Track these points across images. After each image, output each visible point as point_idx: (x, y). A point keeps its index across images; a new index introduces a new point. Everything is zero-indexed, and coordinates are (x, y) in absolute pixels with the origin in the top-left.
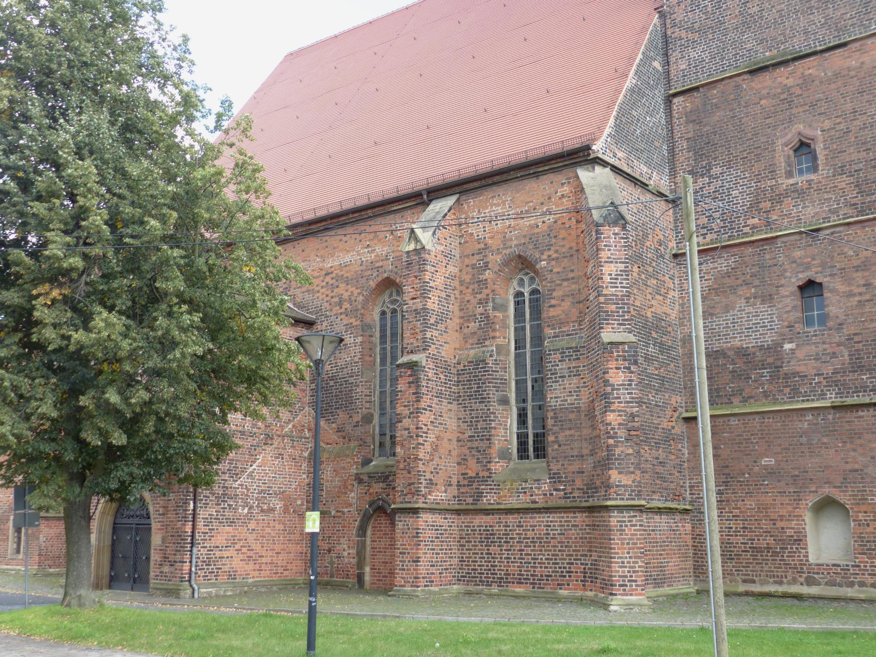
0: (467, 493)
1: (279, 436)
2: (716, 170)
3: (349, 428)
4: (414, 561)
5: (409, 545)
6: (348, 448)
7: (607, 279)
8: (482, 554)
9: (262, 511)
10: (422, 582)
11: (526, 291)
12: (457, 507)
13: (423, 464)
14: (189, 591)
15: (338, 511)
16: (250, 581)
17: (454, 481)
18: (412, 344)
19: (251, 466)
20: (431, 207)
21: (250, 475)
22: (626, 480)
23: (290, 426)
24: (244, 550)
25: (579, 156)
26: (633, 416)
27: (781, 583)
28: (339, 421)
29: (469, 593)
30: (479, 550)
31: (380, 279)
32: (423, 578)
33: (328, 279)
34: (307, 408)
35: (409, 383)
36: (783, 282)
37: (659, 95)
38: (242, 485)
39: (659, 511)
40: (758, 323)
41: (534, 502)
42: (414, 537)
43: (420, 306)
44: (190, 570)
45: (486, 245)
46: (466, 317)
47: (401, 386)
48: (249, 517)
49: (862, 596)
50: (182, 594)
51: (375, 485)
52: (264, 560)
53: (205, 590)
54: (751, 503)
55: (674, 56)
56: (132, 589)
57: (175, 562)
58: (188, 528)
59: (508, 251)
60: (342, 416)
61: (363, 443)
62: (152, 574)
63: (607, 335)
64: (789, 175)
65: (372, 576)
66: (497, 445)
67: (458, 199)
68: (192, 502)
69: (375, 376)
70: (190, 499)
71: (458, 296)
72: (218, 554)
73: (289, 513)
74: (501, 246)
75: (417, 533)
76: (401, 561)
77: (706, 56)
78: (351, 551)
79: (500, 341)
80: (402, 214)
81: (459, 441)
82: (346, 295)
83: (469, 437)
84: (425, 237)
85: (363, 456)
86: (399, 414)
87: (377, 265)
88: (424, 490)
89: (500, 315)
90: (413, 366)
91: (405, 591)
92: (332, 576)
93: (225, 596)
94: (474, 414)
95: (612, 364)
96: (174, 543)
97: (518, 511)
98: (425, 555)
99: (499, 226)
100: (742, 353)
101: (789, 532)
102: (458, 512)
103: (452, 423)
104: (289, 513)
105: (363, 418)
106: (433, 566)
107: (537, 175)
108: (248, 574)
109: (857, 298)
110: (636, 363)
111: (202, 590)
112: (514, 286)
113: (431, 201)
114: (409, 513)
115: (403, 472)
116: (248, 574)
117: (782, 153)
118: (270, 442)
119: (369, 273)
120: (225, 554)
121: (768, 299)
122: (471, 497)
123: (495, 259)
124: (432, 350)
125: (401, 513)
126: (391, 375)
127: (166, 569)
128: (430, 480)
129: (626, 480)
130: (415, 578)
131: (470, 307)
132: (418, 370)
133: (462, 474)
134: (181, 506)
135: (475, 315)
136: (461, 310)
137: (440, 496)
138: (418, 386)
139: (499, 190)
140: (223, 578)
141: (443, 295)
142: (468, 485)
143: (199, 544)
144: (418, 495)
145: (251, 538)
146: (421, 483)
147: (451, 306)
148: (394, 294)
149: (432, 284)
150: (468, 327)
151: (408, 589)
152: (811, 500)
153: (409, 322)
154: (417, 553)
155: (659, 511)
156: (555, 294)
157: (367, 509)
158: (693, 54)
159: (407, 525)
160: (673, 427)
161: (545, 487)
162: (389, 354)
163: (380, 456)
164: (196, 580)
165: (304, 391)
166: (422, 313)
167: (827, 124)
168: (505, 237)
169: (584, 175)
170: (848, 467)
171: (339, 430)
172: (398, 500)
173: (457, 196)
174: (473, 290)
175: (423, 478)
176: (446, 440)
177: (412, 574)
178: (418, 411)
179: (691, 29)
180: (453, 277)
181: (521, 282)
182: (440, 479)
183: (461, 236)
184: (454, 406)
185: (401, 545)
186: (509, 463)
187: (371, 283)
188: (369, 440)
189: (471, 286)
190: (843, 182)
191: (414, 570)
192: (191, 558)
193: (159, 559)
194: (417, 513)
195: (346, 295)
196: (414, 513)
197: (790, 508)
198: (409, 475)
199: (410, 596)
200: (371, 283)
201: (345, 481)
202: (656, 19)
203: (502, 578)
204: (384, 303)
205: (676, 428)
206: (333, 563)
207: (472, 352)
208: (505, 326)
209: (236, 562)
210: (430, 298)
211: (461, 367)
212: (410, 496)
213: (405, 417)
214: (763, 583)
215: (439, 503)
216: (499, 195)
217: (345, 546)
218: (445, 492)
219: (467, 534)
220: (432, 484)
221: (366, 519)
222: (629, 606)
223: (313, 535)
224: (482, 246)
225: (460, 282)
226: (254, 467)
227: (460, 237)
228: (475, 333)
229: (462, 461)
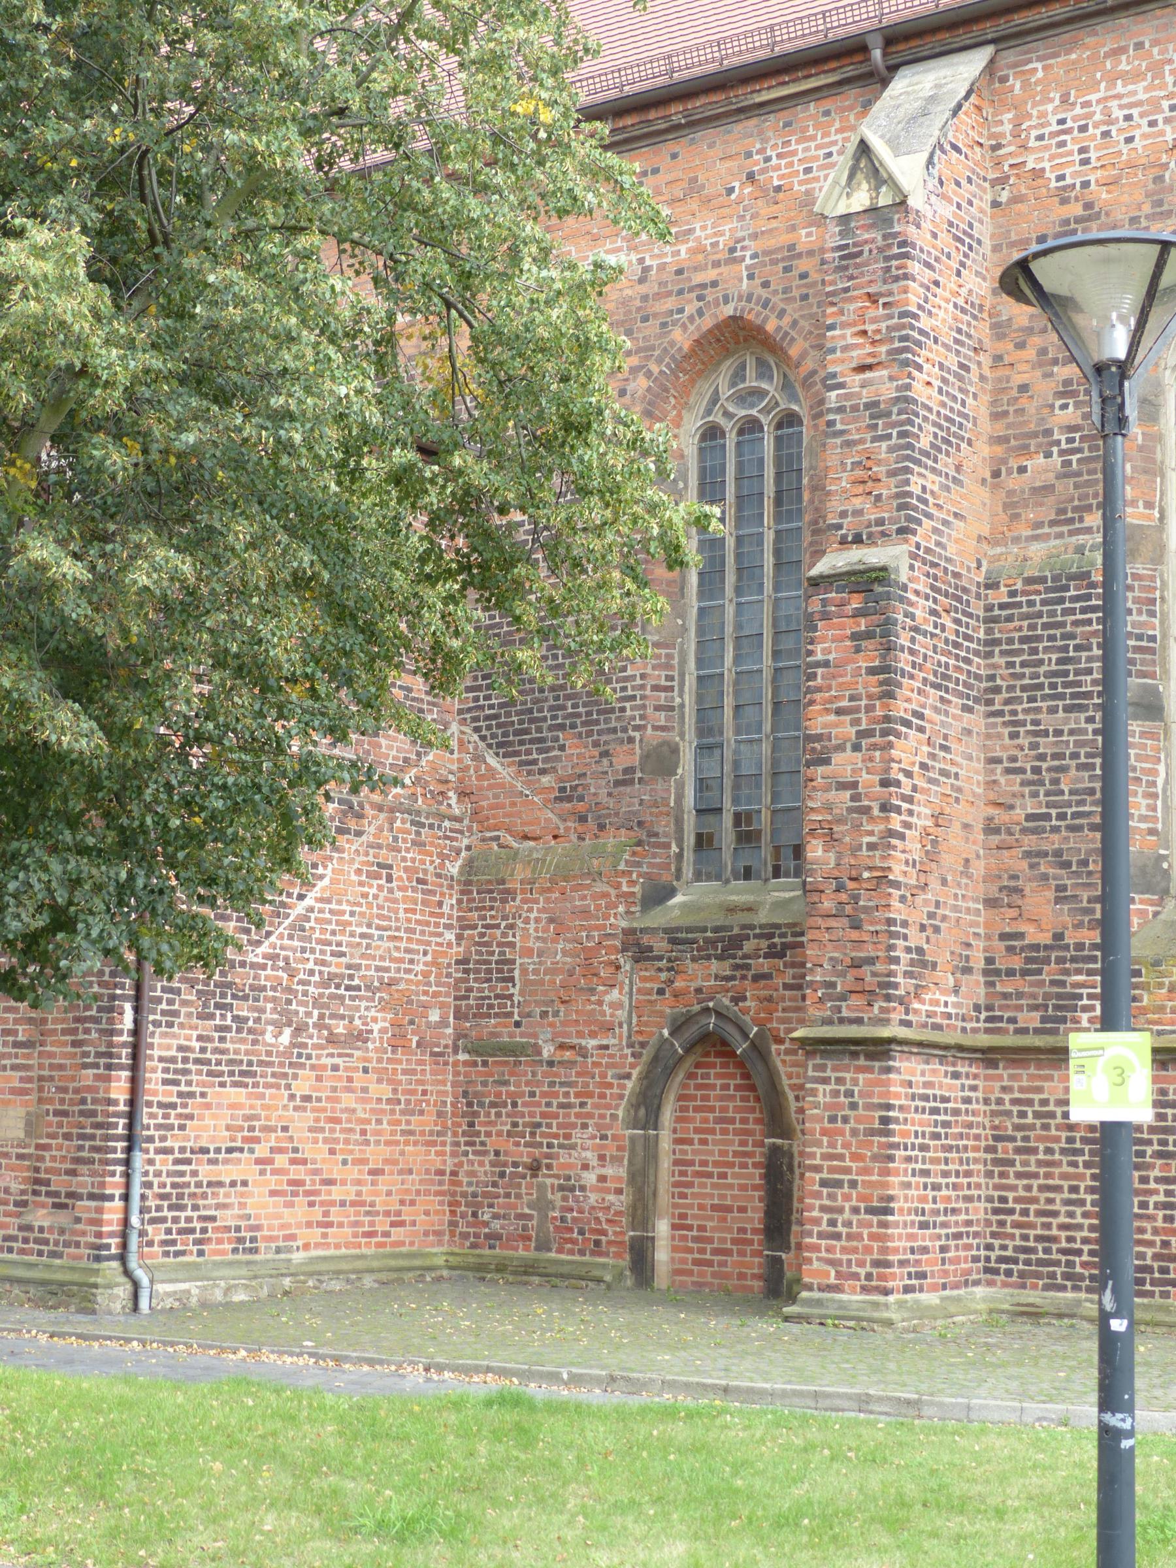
0: (1020, 995)
1: (380, 809)
3: (598, 789)
4: (871, 1211)
5: (856, 1157)
6: (597, 852)
8: (1074, 1189)
9: (332, 1040)
10: (898, 1278)
12: (984, 1040)
13: (903, 899)
14: (123, 1291)
15: (562, 1047)
16: (298, 1257)
18: (858, 513)
19: (301, 897)
20: (900, 84)
21: (298, 928)
24: (281, 1160)
28: (565, 768)
29: (1032, 1314)
30: (1064, 1176)
31: (707, 322)
32: (902, 1263)
34: (454, 727)
35: (855, 637)
38: (274, 957)
42: (872, 1132)
43: (888, 391)
44: (126, 1222)
45: (1088, 206)
47: (828, 645)
48: (296, 1057)
50: (102, 1297)
51: (691, 967)
52: (336, 1193)
53: (169, 1288)
57: (71, 1195)
58: (119, 1090)
60: (575, 752)
61: (645, 835)
65: (675, 1249)
68: (128, 1007)
69: (684, 628)
70: (123, 998)
71: (987, 372)
72: (205, 1172)
74: (1147, 209)
75: (885, 1121)
76: (823, 1209)
78: (609, 1171)
80: (785, 116)
81: (991, 829)
83: (1030, 817)
84: (908, 170)
85: (646, 875)
86: (819, 738)
87: (698, 278)
88: (904, 984)
90: (870, 583)
91: (842, 1305)
92: (543, 1246)
93: (228, 1305)
94: (1046, 745)
96: (67, 1137)
98: (906, 1191)
99: (1137, 143)
102: (989, 1057)
103: (972, 774)
105: (645, 757)
106: (924, 1225)
108: (292, 1237)
111: (161, 1288)
113: (893, 69)
114: (855, 1055)
115: (832, 923)
116: (292, 1237)
118: (353, 825)
119: (670, 303)
120: (226, 1173)
122: (1035, 1008)
124: (923, 535)
125: (825, 1054)
126: (738, 626)
127: (41, 1217)
128: (920, 951)
130: (877, 1264)
131: (1031, 407)
132: (888, 596)
133: (1003, 937)
134: (96, 1020)
135: (1048, 432)
136: (996, 416)
138: (889, 648)
140: (220, 1249)
141: (952, 362)
142: (1025, 973)
143: (150, 1139)
144: (888, 998)
145: (301, 1122)
146: (896, 960)
147: (970, 401)
148: (750, 371)
149: (925, 323)
150: (1022, 470)
151: (852, 1297)
153: (849, 444)
154: (886, 1185)
157: (663, 1041)
159: (849, 1094)
162: (730, 560)
163: (698, 876)
164: (142, 1256)
166: (892, 415)
168: (1159, 179)
171: (564, 796)
172: (814, 1012)
173: (989, 50)
174: (1043, 351)
175: (900, 943)
176: (956, 827)
177: (868, 1250)
178: (888, 727)
182: (942, 953)
183: (1002, 181)
184: (977, 720)
185: (826, 1157)
186: (1160, 903)
187: (677, 334)
188: (665, 826)
189: (1036, 341)
191: (872, 1237)
192: (128, 1185)
193: (15, 1187)
194: (886, 1055)
196: (871, 1056)
198: (854, 935)
199: (863, 1324)
200: (677, 334)
201: (589, 955)
203: (1148, 1269)
204: (715, 400)
206: (551, 1205)
207: (1037, 551)
209: (260, 1203)
210: (919, 368)
211: (1001, 595)
212: (856, 1001)
213: (840, 748)
215: (937, 1027)
216: (1139, 46)
217: (590, 1156)
218: (956, 991)
219: (1018, 1127)
220: (924, 964)
221: (658, 1073)
223: (1109, 1135)
224: (1077, 210)
225: (994, 326)
226: (309, 902)
227: (994, 182)
228: (1048, 489)
229: (1004, 895)
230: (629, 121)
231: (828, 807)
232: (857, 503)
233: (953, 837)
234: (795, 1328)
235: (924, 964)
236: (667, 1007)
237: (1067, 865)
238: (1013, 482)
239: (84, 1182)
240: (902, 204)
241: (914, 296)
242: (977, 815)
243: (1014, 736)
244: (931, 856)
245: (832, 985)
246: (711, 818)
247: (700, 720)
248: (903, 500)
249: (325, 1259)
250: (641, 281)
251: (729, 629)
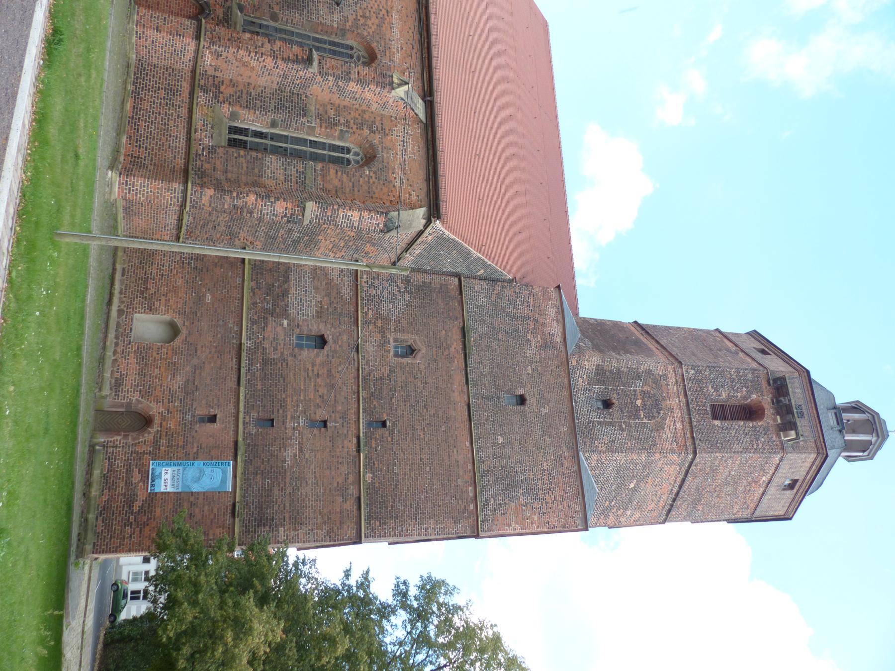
2: (407, 297)
10: (140, 30)
11: (350, 156)
12: (198, 72)
17: (218, 74)
20: (421, 101)
22: (205, 200)
25: (434, 211)
26: (251, 213)
27: (121, 293)
29: (128, 66)
31: (377, 51)
33: (384, 12)
36: (328, 326)
39: (180, 220)
41: (196, 131)
46: (338, 110)
47: (296, 49)
49: (108, 343)
54: (180, 282)
59: (380, 149)
63: (310, 206)
64: (396, 340)
66: (243, 112)
67: (421, 122)
77: (480, 303)
79: (318, 130)
82: (369, 22)
89: (336, 134)
90: (309, 61)
95: (289, 205)
97: (190, 117)
100: (285, 294)
101: (157, 304)
102: (194, 71)
103: (263, 81)
105: (275, 13)
113: (425, 102)
117: (410, 338)
119: (383, 44)
121: (319, 315)
123: (376, 139)
129: (205, 200)
136: (344, 107)
137: (208, 60)
139: (423, 152)
148: (364, 60)
151: (135, 17)
152: (178, 321)
155: (180, 220)
161: (206, 141)
166: (347, 76)
167: (422, 367)
169: (421, 212)
170: (199, 347)
172: (208, 26)
176: (250, 74)
179: (498, 297)
180: (369, 106)
181: (356, 154)
183: (396, 119)
184: (275, 86)
188: (258, 14)
189: (360, 118)
190: (385, 371)
195: (369, 22)
197: (174, 307)
207: (313, 108)
208: (327, 137)
212: (210, 36)
214: (122, 282)
222: (110, 185)
224: (387, 132)
228: (326, 113)
229: (233, 84)
233: (248, 73)
238: (329, 107)
240: (393, 89)
241: (372, 87)
242: (252, 81)
244: (244, 64)
248: (327, 74)
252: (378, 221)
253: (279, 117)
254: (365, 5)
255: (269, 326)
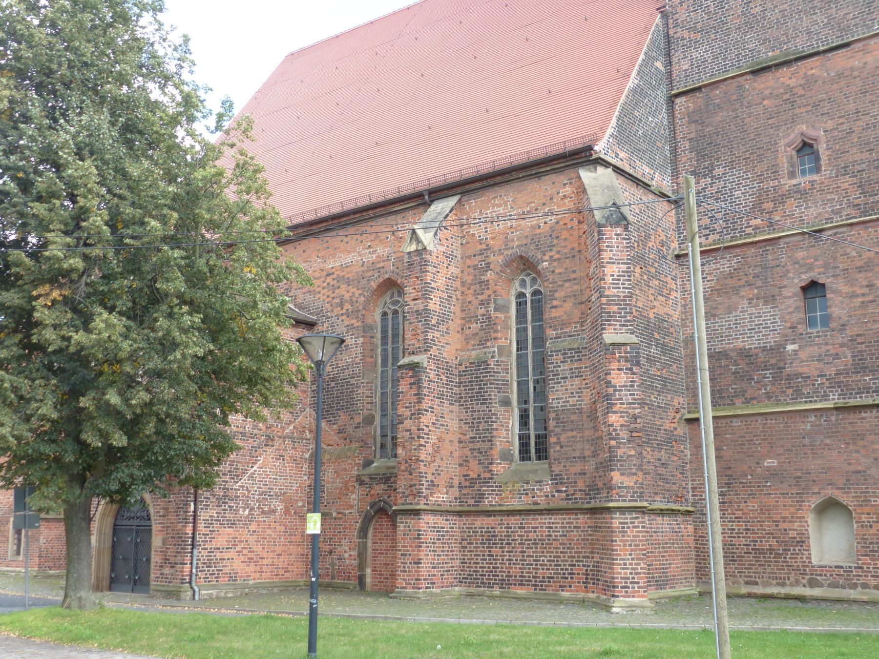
0: (468, 494)
2: (719, 171)
3: (350, 429)
4: (415, 563)
5: (411, 546)
6: (349, 450)
7: (609, 279)
8: (484, 555)
9: (263, 512)
10: (423, 584)
11: (528, 292)
12: (458, 509)
13: (425, 465)
14: (190, 593)
15: (339, 513)
16: (251, 582)
17: (456, 482)
18: (413, 345)
19: (252, 467)
20: (433, 207)
21: (251, 477)
22: (628, 482)
23: (291, 427)
24: (245, 551)
25: (581, 156)
26: (635, 417)
27: (783, 585)
28: (340, 423)
29: (471, 595)
30: (481, 551)
31: (381, 280)
32: (425, 579)
33: (329, 280)
34: (308, 409)
35: (410, 384)
36: (785, 282)
37: (661, 95)
38: (243, 487)
39: (662, 512)
40: (760, 324)
41: (536, 504)
42: (415, 539)
43: (421, 307)
44: (191, 571)
45: (487, 245)
46: (468, 319)
47: (403, 387)
48: (250, 518)
49: (865, 598)
50: (183, 595)
51: (376, 487)
52: (265, 562)
54: (753, 505)
55: (676, 56)
56: (133, 591)
58: (189, 530)
59: (509, 252)
60: (343, 417)
61: (364, 445)
62: (152, 576)
63: (609, 336)
64: (792, 175)
65: (373, 578)
68: (192, 504)
69: (376, 377)
70: (191, 501)
71: (459, 297)
72: (219, 556)
73: (290, 514)
74: (503, 247)
75: (419, 535)
76: (402, 563)
77: (708, 56)
78: (352, 553)
79: (502, 342)
80: (403, 214)
81: (460, 442)
82: (347, 296)
83: (471, 438)
84: (426, 238)
85: (364, 457)
86: (400, 416)
87: (378, 266)
88: (425, 492)
89: (501, 316)
90: (414, 367)
91: (407, 593)
92: (333, 578)
93: (225, 598)
94: (476, 415)
95: (614, 366)
96: (175, 545)
97: (520, 512)
98: (427, 557)
99: (501, 226)
100: (745, 354)
101: (792, 534)
102: (459, 514)
103: (453, 425)
104: (290, 514)
105: (364, 419)
107: (539, 175)
108: (249, 576)
109: (860, 299)
110: (638, 364)
111: (203, 592)
112: (516, 287)
113: (432, 201)
114: (410, 514)
116: (249, 576)
117: (785, 154)
118: (271, 444)
119: (370, 273)
120: (226, 556)
121: (770, 299)
122: (472, 498)
123: (497, 260)
124: (434, 351)
125: (402, 514)
126: (393, 376)
127: (167, 571)
128: (432, 481)
129: (628, 482)
130: (417, 580)
131: (472, 308)
133: (464, 476)
135: (477, 316)
136: (463, 311)
137: (441, 497)
138: (420, 388)
139: (501, 191)
140: (224, 580)
141: (445, 296)
142: (470, 487)
143: (200, 545)
144: (420, 497)
146: (423, 485)
147: (452, 307)
148: (396, 295)
149: (433, 285)
150: (470, 328)
151: (409, 590)
152: (814, 502)
153: (411, 323)
154: (419, 555)
155: (662, 512)
156: (557, 295)
157: (368, 511)
158: (695, 54)
159: (409, 527)
160: (675, 429)
162: (390, 355)
163: (381, 457)
164: (196, 582)
165: (305, 392)
167: (830, 124)
168: (506, 238)
169: (586, 175)
170: (851, 468)
171: (340, 432)
172: (399, 501)
173: (458, 197)
174: (475, 291)
175: (424, 479)
176: (447, 442)
177: (414, 575)
178: (419, 412)
179: (693, 29)
180: (454, 278)
181: (523, 283)
183: (463, 237)
184: (456, 408)
186: (510, 464)
187: (372, 283)
188: (370, 441)
189: (473, 287)
190: (846, 182)
191: (415, 571)
192: (192, 560)
193: (159, 561)
194: (418, 514)
195: (347, 296)
196: (415, 515)
197: (792, 510)
198: (410, 477)
199: (411, 598)
200: (372, 283)
201: (347, 483)
202: (658, 19)
204: (385, 303)
205: (679, 429)
206: (335, 565)
207: (474, 353)
208: (507, 327)
209: (237, 564)
210: (431, 299)
211: (463, 368)
212: (411, 497)
213: (406, 419)
216: (501, 196)
217: (346, 548)
218: (447, 494)
219: (468, 536)
220: (434, 485)
221: (367, 521)
222: (631, 608)
223: (314, 537)
224: (484, 246)
226: (255, 468)
227: (462, 237)
228: (477, 334)
229: (464, 463)
230: (358, 215)
231: (403, 437)
232: (413, 342)
234: (391, 600)
235: (434, 485)
236: (369, 500)
237: (481, 453)
239: (179, 559)
241: (429, 277)
243: (466, 412)
245: (404, 493)
246: (385, 438)
247: (382, 406)
249: (261, 583)
250: (362, 266)
251: (390, 377)
252: (612, 233)
253: (495, 396)
254: (327, 306)
255: (800, 370)
